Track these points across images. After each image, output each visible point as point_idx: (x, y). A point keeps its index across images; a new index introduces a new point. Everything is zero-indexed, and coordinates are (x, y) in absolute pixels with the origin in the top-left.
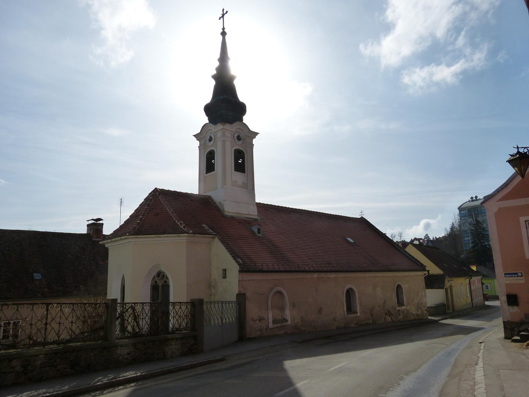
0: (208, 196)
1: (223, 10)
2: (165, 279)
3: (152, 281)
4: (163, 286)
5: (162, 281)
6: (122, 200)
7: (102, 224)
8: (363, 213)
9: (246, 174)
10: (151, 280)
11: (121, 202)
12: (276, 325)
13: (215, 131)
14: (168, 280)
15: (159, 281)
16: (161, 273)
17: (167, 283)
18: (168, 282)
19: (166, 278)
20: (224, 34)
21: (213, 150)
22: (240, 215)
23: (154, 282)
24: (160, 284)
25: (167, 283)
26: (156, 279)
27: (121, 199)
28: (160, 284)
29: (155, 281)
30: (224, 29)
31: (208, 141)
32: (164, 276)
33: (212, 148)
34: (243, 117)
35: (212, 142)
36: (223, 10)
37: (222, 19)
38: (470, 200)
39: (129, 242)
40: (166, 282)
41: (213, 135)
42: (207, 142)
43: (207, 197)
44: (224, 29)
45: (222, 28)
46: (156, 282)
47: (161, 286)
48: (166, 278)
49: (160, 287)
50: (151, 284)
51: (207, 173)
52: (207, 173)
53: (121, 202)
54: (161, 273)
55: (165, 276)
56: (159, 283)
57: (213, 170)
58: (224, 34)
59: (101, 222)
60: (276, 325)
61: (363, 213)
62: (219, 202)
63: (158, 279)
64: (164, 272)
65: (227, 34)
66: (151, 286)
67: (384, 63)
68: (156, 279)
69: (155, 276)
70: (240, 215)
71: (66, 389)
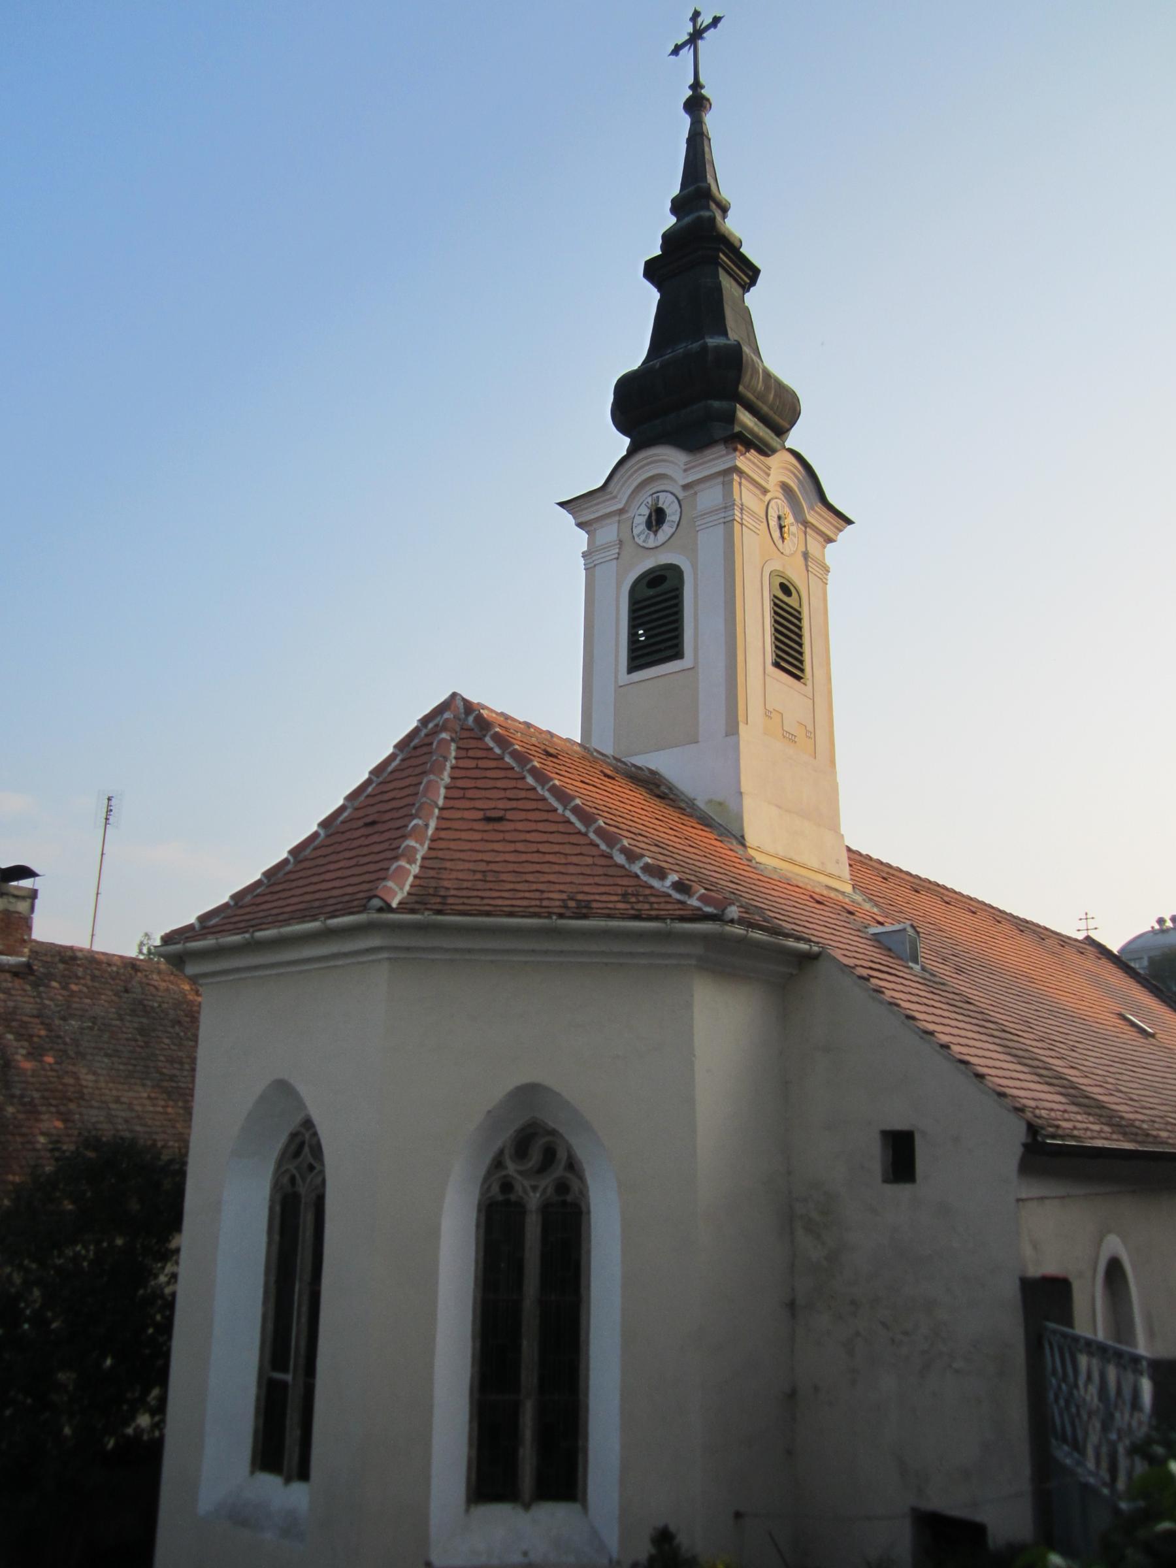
0: (649, 770)
1: (697, 14)
2: (558, 1171)
4: (546, 1208)
5: (547, 1182)
6: (113, 802)
7: (33, 894)
8: (1091, 923)
9: (808, 690)
11: (109, 811)
13: (690, 480)
14: (581, 1178)
18: (581, 1192)
20: (696, 104)
21: (671, 565)
22: (797, 869)
24: (534, 1201)
26: (511, 1168)
27: (109, 799)
28: (534, 1201)
30: (696, 86)
31: (643, 527)
32: (550, 1155)
33: (664, 558)
35: (666, 530)
36: (697, 14)
37: (687, 54)
38: (1157, 927)
39: (803, 894)
40: (562, 1187)
41: (673, 498)
42: (636, 532)
43: (647, 773)
44: (696, 86)
45: (691, 81)
46: (507, 1186)
51: (632, 669)
52: (632, 669)
53: (109, 811)
55: (562, 1155)
56: (525, 1191)
57: (676, 653)
58: (696, 104)
59: (26, 883)
61: (1091, 923)
62: (710, 801)
64: (553, 1133)
68: (511, 1168)
69: (501, 1152)
70: (797, 869)
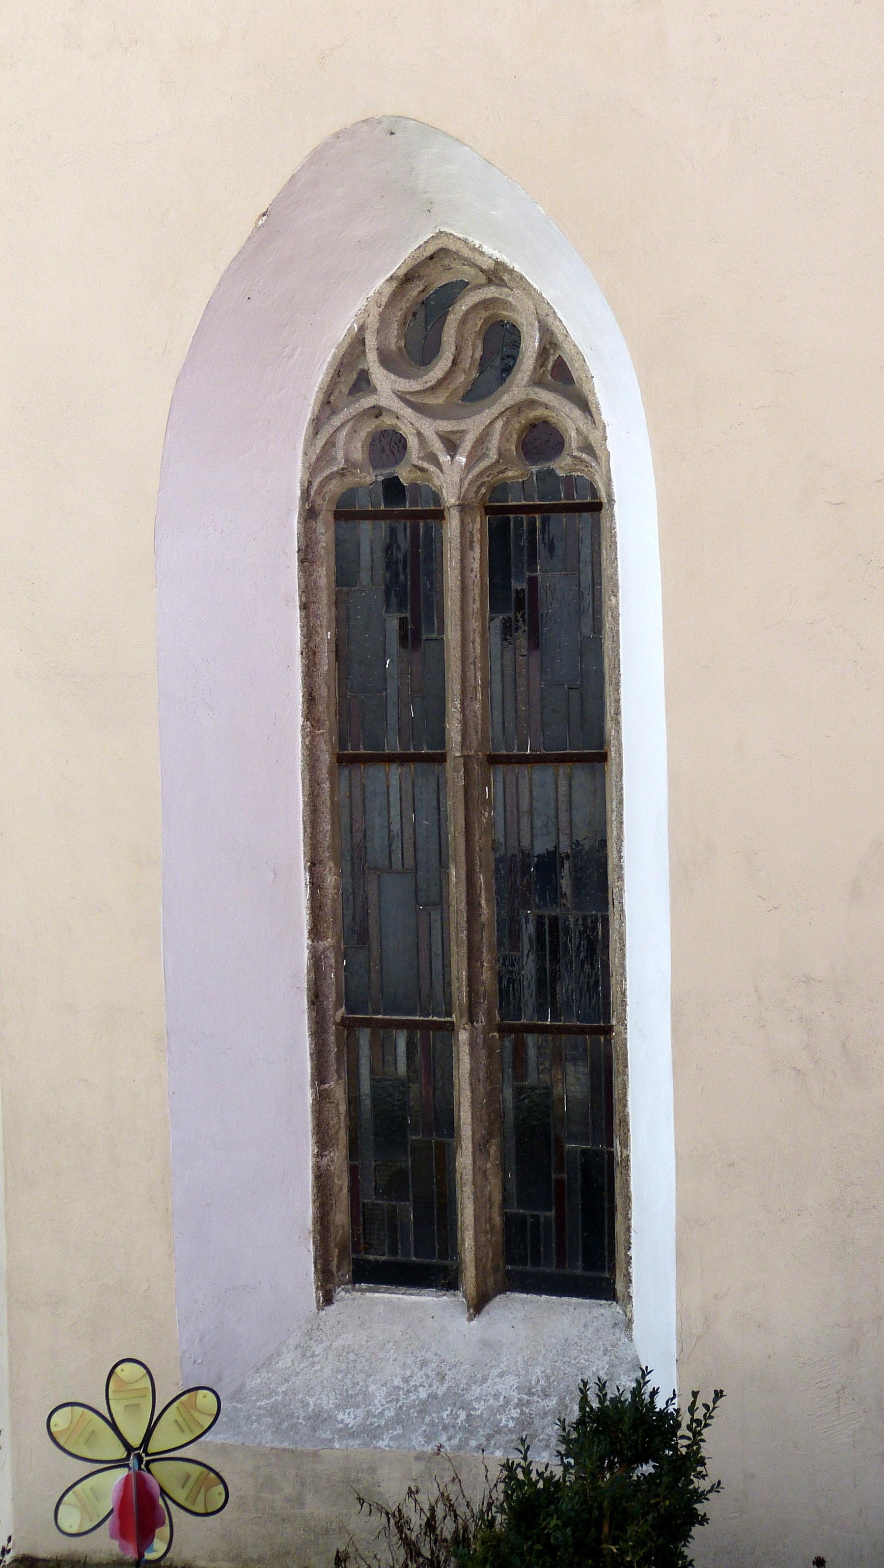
3: (317, 424)
10: (309, 412)
12: (361, 1204)
14: (584, 405)
15: (430, 427)
16: (457, 288)
17: (561, 466)
18: (588, 448)
19: (537, 382)
23: (358, 453)
25: (561, 466)
29: (370, 426)
34: (118, 1542)
47: (464, 508)
48: (537, 382)
49: (452, 527)
50: (313, 469)
54: (457, 288)
55: (531, 344)
56: (433, 458)
60: (361, 1204)
63: (405, 385)
65: (819, 1555)
66: (309, 514)
67: (635, 1386)
71: (517, 453)
